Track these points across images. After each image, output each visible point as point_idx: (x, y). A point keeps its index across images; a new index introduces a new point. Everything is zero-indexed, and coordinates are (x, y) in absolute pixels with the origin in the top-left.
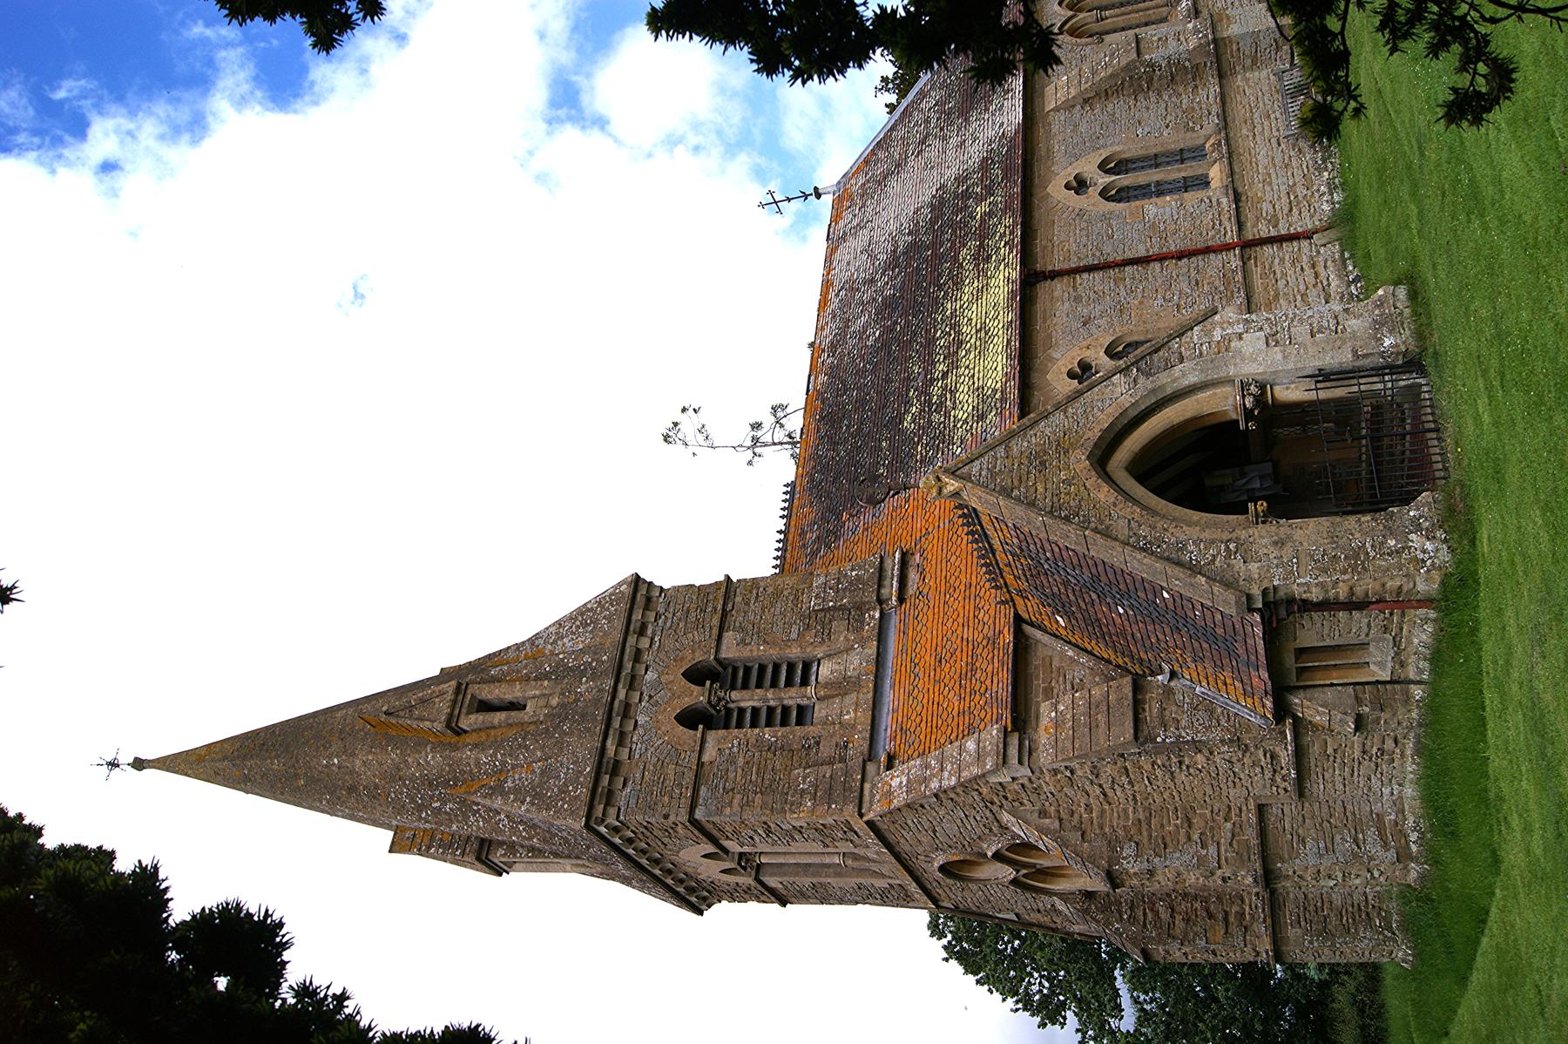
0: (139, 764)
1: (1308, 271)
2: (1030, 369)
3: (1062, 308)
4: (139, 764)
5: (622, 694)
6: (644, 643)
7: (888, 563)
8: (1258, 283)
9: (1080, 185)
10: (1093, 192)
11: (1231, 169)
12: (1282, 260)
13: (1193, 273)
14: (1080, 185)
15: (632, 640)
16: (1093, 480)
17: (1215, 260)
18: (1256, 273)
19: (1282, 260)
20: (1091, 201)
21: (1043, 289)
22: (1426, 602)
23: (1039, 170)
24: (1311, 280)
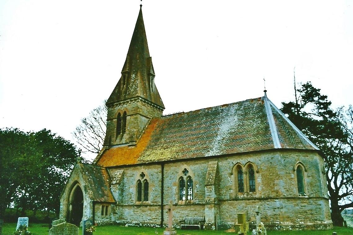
0: (141, 6)
1: (155, 217)
2: (239, 155)
3: (156, 170)
4: (141, 6)
5: (122, 102)
6: (130, 102)
7: (134, 142)
8: (154, 208)
9: (185, 171)
10: (183, 175)
11: (257, 199)
12: (158, 213)
13: (159, 196)
14: (185, 171)
15: (129, 100)
16: (298, 162)
17: (160, 200)
18: (157, 208)
19: (158, 213)
20: (181, 174)
21: (160, 166)
22: (343, 198)
23: (192, 162)
24: (153, 217)
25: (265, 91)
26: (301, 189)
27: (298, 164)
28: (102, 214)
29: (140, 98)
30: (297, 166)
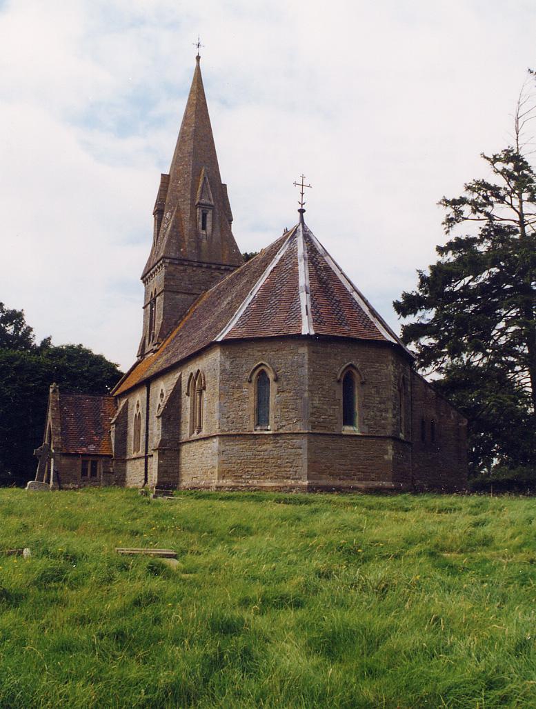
0: (198, 58)
4: (198, 58)
25: (302, 211)
26: (261, 418)
27: (261, 368)
28: (84, 472)
29: (168, 261)
30: (258, 371)
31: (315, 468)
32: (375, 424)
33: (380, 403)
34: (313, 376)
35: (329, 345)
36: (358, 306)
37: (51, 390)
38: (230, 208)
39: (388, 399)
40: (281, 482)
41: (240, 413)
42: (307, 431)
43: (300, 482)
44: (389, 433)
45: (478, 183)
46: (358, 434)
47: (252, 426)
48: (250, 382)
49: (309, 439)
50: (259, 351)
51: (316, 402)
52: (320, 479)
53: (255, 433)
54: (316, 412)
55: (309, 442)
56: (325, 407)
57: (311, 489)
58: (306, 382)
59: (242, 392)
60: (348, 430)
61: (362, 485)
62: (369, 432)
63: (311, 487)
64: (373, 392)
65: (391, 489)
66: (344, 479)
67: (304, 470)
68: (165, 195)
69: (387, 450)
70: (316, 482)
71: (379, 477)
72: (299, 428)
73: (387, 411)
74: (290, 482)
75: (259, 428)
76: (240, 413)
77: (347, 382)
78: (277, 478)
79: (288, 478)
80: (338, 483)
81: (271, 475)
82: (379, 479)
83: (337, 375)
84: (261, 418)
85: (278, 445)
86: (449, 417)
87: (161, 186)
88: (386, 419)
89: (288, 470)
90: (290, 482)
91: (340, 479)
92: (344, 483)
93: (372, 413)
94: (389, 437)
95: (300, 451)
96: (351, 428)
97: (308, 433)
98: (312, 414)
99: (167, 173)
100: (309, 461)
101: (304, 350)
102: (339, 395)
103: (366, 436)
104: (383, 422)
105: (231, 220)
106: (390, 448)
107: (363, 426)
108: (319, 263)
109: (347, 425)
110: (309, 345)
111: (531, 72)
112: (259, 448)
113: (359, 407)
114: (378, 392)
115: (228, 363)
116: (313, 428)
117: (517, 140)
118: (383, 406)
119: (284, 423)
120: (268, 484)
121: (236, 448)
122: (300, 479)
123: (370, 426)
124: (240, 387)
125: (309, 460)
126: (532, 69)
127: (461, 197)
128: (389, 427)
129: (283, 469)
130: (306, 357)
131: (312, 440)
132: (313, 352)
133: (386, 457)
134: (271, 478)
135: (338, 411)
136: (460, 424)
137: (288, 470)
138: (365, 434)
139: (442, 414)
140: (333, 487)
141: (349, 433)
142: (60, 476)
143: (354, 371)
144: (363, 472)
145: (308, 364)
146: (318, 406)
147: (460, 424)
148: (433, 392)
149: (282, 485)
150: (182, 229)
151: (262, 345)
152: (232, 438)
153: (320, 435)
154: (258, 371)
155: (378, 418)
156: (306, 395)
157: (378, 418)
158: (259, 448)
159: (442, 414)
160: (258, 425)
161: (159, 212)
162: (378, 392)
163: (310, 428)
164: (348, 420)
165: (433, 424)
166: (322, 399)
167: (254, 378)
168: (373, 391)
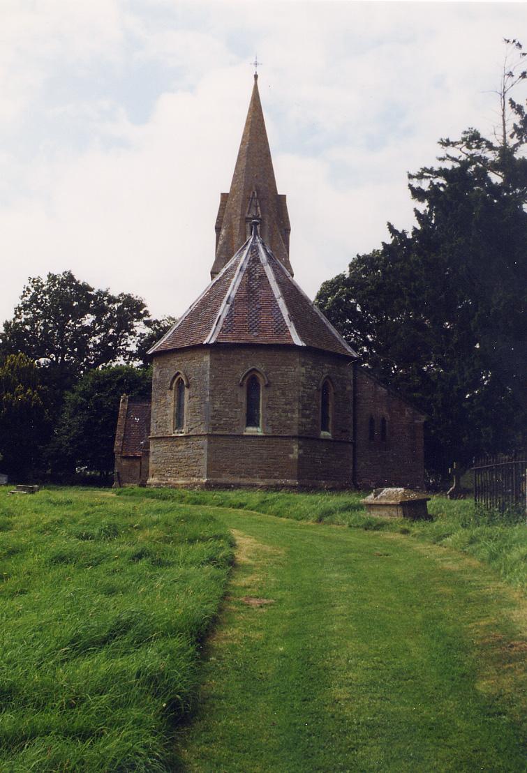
0: (256, 77)
4: (256, 77)
26: (179, 423)
30: (177, 379)
31: (213, 468)
32: (280, 424)
33: (286, 405)
34: (215, 382)
35: (233, 352)
36: (280, 311)
37: (121, 400)
38: (288, 222)
39: (295, 400)
40: (189, 480)
41: (164, 418)
42: (206, 433)
43: (201, 479)
44: (295, 432)
45: (425, 170)
46: (261, 434)
47: (172, 429)
48: (171, 389)
49: (209, 441)
50: (178, 361)
51: (217, 406)
52: (220, 476)
53: (173, 435)
54: (217, 414)
55: (209, 442)
56: (227, 410)
57: (208, 486)
58: (208, 387)
59: (166, 398)
60: (251, 430)
61: (261, 483)
62: (273, 432)
63: (209, 484)
64: (278, 394)
65: (295, 487)
66: (244, 477)
67: (204, 469)
68: (223, 213)
69: (293, 449)
70: (214, 479)
71: (283, 475)
72: (202, 430)
73: (293, 411)
74: (195, 480)
75: (176, 431)
76: (164, 418)
77: (252, 384)
78: (187, 476)
79: (194, 476)
80: (238, 480)
81: (182, 474)
82: (283, 477)
83: (239, 379)
84: (179, 423)
85: (189, 446)
86: (403, 414)
87: (221, 205)
88: (292, 419)
89: (194, 468)
90: (195, 480)
91: (241, 477)
92: (245, 481)
93: (277, 414)
94: (294, 437)
95: (203, 452)
96: (255, 429)
97: (207, 434)
98: (213, 417)
99: (227, 191)
100: (208, 461)
101: (207, 358)
102: (243, 399)
103: (269, 437)
104: (289, 422)
105: (288, 230)
106: (295, 448)
107: (266, 427)
108: (256, 273)
109: (251, 426)
110: (211, 353)
111: (508, 41)
112: (176, 449)
113: (262, 410)
114: (283, 394)
115: (158, 373)
116: (214, 429)
117: (503, 116)
118: (288, 407)
119: (193, 426)
120: (180, 482)
121: (161, 449)
122: (201, 477)
123: (273, 427)
124: (165, 394)
125: (209, 459)
126: (507, 39)
127: (284, 197)
128: (294, 427)
129: (190, 468)
130: (209, 364)
131: (212, 441)
132: (216, 359)
133: (291, 456)
134: (183, 476)
135: (241, 413)
136: (416, 421)
137: (194, 468)
138: (267, 435)
139: (394, 412)
140: (232, 484)
141: (250, 434)
142: (121, 476)
143: (258, 375)
144: (265, 470)
145: (210, 371)
146: (219, 409)
147: (416, 421)
148: (383, 389)
149: (189, 482)
150: (232, 245)
151: (179, 355)
152: (160, 440)
153: (220, 436)
154: (177, 379)
155: (283, 419)
156: (207, 399)
157: (283, 419)
158: (176, 449)
159: (394, 412)
160: (176, 428)
161: (218, 229)
162: (283, 394)
163: (211, 430)
164: (252, 420)
165: (384, 421)
166: (223, 402)
167: (245, 382)
168: (278, 393)
